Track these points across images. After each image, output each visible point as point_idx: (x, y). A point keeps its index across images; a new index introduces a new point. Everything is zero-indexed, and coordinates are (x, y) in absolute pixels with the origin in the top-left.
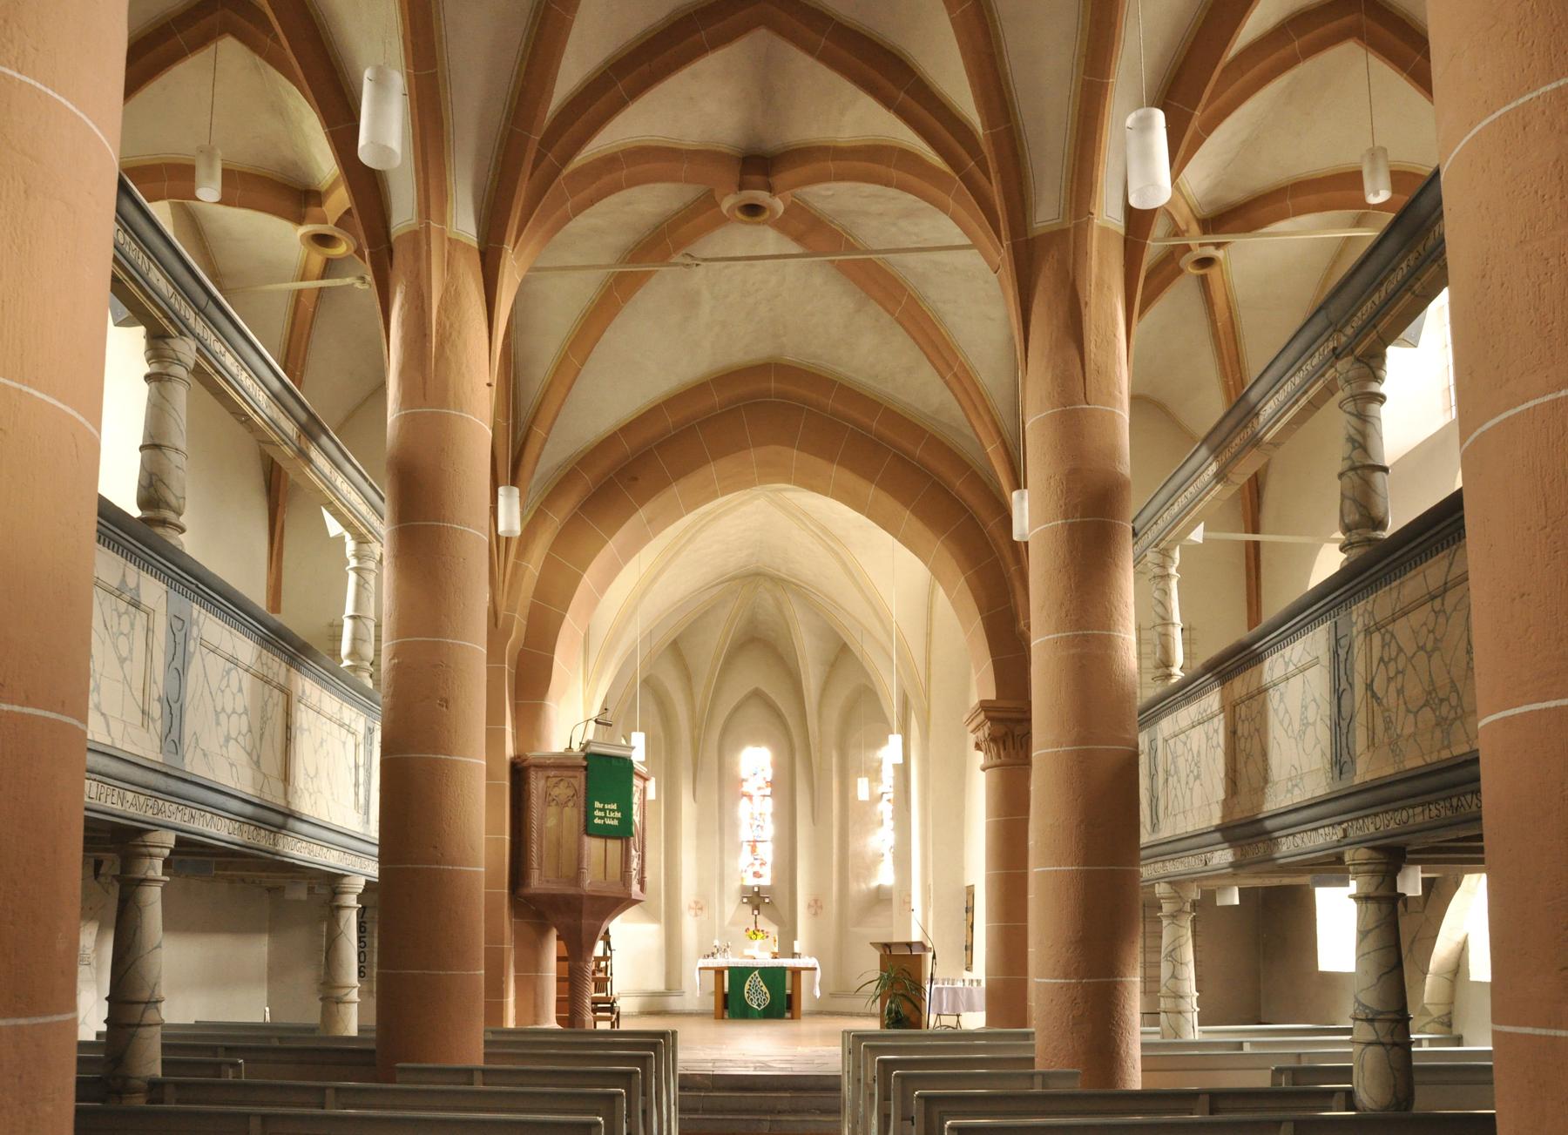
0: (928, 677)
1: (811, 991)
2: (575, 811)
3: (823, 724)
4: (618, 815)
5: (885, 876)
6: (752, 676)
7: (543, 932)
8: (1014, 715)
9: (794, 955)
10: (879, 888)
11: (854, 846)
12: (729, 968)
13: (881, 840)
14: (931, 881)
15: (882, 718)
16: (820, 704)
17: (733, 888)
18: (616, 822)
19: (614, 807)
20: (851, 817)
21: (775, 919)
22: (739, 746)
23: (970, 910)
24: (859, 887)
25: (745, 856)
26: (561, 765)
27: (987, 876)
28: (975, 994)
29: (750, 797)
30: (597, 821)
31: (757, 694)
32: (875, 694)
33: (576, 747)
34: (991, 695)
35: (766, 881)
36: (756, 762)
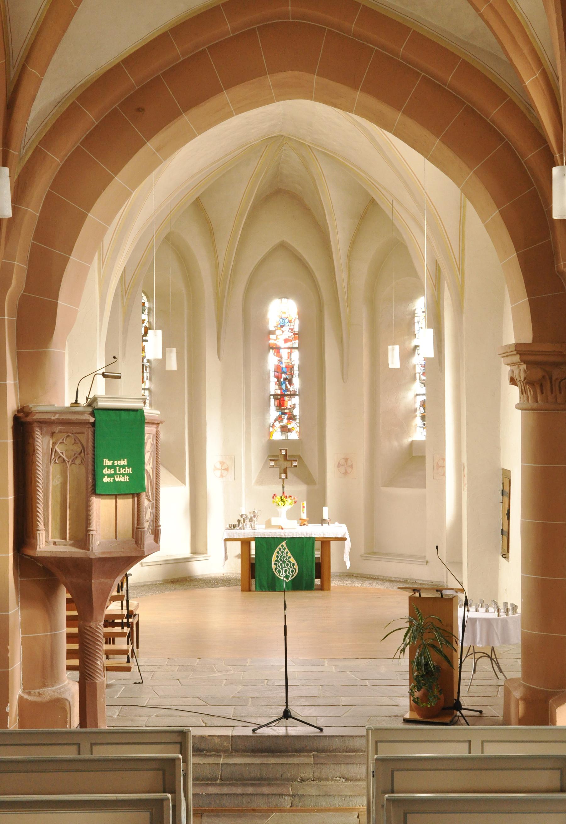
0: (462, 250)
1: (341, 559)
2: (83, 468)
4: (129, 471)
5: (418, 433)
6: (278, 228)
7: (50, 591)
8: (551, 359)
12: (255, 539)
14: (464, 460)
15: (412, 271)
16: (350, 257)
18: (126, 479)
19: (124, 462)
21: (307, 478)
23: (506, 494)
24: (391, 446)
26: (65, 424)
27: (523, 467)
28: (511, 626)
30: (106, 480)
32: (406, 247)
33: (82, 401)
34: (527, 337)
35: (293, 436)
36: (282, 312)
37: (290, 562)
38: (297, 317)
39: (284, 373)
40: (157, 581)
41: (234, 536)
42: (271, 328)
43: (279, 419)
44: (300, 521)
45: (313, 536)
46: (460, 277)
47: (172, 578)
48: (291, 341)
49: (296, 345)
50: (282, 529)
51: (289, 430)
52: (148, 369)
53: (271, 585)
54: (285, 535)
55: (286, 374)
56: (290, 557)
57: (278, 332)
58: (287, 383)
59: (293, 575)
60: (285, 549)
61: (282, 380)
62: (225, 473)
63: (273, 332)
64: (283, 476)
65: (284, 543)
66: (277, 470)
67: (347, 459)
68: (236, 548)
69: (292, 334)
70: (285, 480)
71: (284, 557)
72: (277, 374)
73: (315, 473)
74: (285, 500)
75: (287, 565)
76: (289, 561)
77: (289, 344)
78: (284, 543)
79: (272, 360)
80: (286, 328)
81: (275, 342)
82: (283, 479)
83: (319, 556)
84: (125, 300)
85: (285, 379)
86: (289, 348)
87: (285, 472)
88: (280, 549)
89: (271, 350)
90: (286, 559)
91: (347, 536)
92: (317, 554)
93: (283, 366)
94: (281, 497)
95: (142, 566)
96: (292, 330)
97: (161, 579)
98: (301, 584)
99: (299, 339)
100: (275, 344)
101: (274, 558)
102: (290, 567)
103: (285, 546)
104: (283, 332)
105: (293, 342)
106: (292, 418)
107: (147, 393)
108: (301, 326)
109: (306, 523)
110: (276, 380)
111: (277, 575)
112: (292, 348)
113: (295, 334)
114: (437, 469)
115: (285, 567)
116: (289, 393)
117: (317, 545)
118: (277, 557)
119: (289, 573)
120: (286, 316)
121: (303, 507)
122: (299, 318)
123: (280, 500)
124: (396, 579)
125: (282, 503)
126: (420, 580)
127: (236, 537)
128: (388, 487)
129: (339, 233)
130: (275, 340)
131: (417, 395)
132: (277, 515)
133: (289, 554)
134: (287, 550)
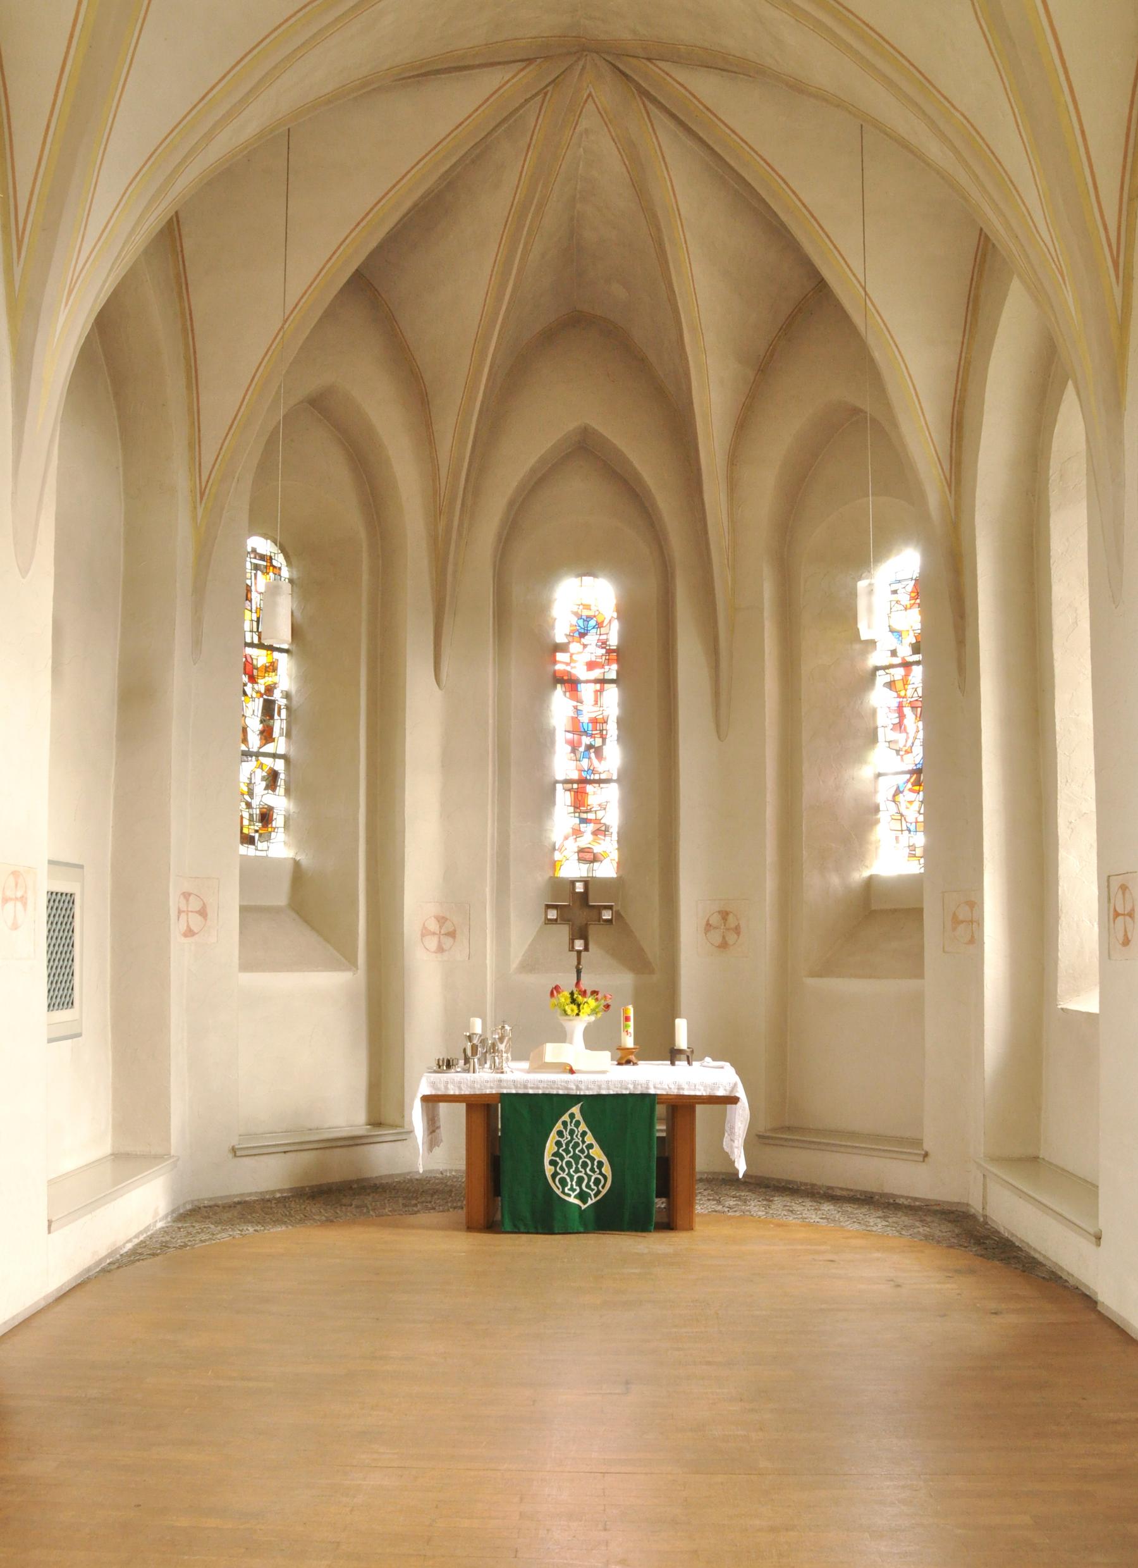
3: (742, 505)
5: (893, 853)
6: (568, 403)
9: (673, 1055)
10: (870, 884)
11: (811, 788)
13: (886, 766)
16: (734, 458)
17: (529, 887)
20: (818, 719)
21: (633, 958)
22: (548, 570)
24: (824, 886)
25: (562, 817)
29: (571, 683)
31: (586, 448)
35: (607, 870)
36: (584, 603)
37: (592, 1159)
38: (615, 615)
39: (586, 733)
40: (274, 1192)
41: (446, 1088)
42: (560, 637)
43: (577, 833)
44: (619, 1054)
45: (652, 1091)
46: (1117, 292)
47: (314, 1183)
48: (603, 667)
49: (613, 676)
50: (572, 1072)
51: (595, 859)
52: (284, 713)
53: (546, 1217)
54: (578, 1088)
55: (592, 736)
56: (590, 1146)
57: (575, 647)
58: (593, 755)
59: (598, 1192)
60: (578, 1124)
61: (582, 749)
62: (447, 942)
63: (562, 648)
64: (579, 945)
65: (576, 1110)
66: (564, 931)
67: (727, 913)
68: (454, 1118)
69: (604, 651)
70: (583, 954)
71: (576, 1145)
72: (570, 736)
73: (652, 948)
74: (580, 999)
75: (585, 1165)
76: (588, 1156)
77: (597, 673)
78: (576, 1110)
79: (560, 706)
80: (591, 639)
81: (568, 668)
82: (579, 952)
83: (664, 1134)
84: (200, 511)
85: (589, 747)
86: (596, 681)
87: (584, 936)
88: (565, 1124)
89: (559, 686)
90: (582, 1151)
91: (741, 1093)
92: (660, 1129)
93: (584, 719)
94: (572, 994)
95: (235, 1156)
96: (603, 644)
97: (286, 1187)
98: (617, 1214)
99: (618, 661)
100: (568, 673)
101: (550, 1147)
102: (592, 1170)
103: (578, 1117)
104: (585, 646)
105: (607, 668)
106: (601, 831)
107: (279, 765)
108: (624, 636)
109: (632, 1058)
110: (569, 748)
111: (558, 1192)
112: (603, 681)
113: (609, 652)
114: (954, 929)
115: (577, 1171)
116: (597, 777)
117: (660, 1110)
118: (558, 1144)
119: (588, 1186)
120: (591, 613)
121: (627, 1019)
122: (618, 618)
123: (569, 1001)
124: (845, 1193)
125: (575, 1007)
126: (907, 1198)
127: (452, 1093)
128: (821, 976)
129: (713, 397)
130: (568, 664)
131: (879, 775)
132: (562, 1037)
133: (590, 1139)
134: (583, 1127)
